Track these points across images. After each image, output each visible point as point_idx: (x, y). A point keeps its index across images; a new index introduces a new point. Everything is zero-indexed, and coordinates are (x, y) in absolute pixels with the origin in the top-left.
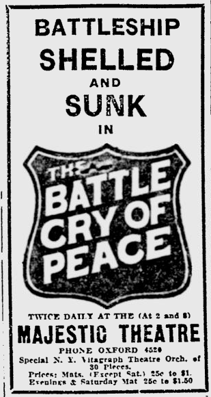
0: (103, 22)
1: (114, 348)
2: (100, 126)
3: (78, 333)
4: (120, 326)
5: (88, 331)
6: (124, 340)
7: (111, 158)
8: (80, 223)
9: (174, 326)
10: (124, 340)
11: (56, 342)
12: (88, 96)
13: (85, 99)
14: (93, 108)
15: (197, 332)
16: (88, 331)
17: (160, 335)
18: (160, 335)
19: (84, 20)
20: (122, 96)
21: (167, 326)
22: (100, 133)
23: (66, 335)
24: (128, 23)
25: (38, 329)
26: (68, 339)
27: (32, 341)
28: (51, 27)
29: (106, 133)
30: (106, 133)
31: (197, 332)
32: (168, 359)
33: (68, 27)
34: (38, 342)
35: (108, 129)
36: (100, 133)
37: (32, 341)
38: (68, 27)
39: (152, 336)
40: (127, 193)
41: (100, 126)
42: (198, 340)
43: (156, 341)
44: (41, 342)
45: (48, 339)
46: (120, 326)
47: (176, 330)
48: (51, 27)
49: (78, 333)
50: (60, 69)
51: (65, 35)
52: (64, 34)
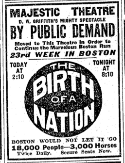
0: (72, 35)
1: (87, 139)
2: (114, 64)
3: (46, 12)
4: (72, 8)
8: (60, 77)
9: (101, 8)
11: (34, 16)
13: (66, 121)
17: (97, 31)
18: (97, 31)
20: (83, 8)
21: (98, 8)
23: (39, 13)
24: (40, 12)
27: (20, 15)
28: (20, 65)
34: (24, 17)
37: (20, 15)
39: (91, 12)
41: (114, 64)
42: (114, 14)
43: (92, 14)
44: (26, 16)
45: (30, 14)
46: (72, 8)
47: (102, 10)
48: (20, 65)
49: (46, 12)
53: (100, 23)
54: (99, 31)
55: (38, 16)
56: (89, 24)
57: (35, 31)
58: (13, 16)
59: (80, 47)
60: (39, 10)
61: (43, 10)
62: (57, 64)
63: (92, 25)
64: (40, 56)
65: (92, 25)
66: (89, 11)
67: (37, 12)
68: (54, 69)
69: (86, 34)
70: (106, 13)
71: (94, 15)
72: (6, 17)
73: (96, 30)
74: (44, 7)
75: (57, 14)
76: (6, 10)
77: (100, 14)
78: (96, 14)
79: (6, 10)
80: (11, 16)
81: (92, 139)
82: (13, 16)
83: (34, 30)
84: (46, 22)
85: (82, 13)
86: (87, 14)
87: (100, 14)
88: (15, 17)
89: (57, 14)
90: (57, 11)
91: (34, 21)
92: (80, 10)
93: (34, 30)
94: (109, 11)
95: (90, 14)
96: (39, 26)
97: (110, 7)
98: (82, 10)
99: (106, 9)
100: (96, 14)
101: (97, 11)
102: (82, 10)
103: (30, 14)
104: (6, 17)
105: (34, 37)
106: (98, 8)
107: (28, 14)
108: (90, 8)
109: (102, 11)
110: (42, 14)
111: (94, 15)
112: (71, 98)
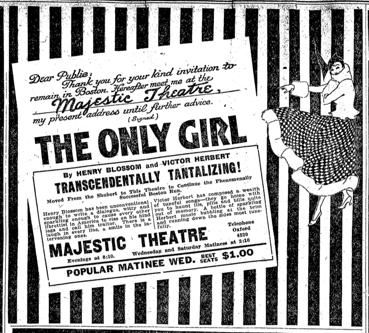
3: (103, 244)
5: (110, 243)
6: (144, 245)
7: (357, 112)
10: (144, 245)
12: (169, 124)
14: (90, 272)
16: (110, 243)
19: (235, 257)
22: (172, 179)
24: (94, 244)
25: (67, 245)
26: (94, 249)
29: (147, 267)
30: (147, 267)
32: (234, 230)
33: (134, 266)
35: (174, 261)
36: (172, 179)
38: (134, 266)
40: (163, 299)
43: (171, 243)
44: (71, 254)
45: (78, 250)
49: (103, 244)
50: (207, 239)
51: (251, 177)
52: (229, 154)
55: (90, 252)
58: (126, 184)
59: (171, 191)
60: (92, 242)
61: (99, 241)
66: (164, 238)
67: (88, 247)
69: (124, 183)
70: (193, 238)
71: (68, 255)
75: (121, 245)
77: (183, 241)
78: (177, 242)
80: (52, 256)
81: (110, 228)
82: (126, 184)
84: (80, 215)
85: (154, 243)
86: (162, 244)
87: (183, 241)
88: (123, 270)
89: (121, 245)
90: (121, 241)
92: (190, 234)
94: (198, 234)
95: (166, 243)
98: (153, 236)
99: (192, 233)
100: (177, 242)
101: (179, 236)
102: (153, 236)
103: (78, 250)
106: (134, 263)
107: (75, 251)
108: (165, 233)
109: (186, 235)
110: (97, 248)
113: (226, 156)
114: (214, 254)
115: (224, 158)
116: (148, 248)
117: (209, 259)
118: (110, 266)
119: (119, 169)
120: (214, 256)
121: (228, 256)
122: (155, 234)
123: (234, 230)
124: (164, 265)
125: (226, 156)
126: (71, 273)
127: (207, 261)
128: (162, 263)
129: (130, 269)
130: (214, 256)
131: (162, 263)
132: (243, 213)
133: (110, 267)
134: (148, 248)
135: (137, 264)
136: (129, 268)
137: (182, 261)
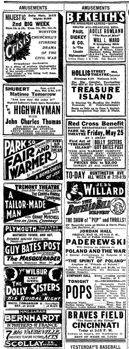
6: (44, 123)
10: (44, 123)
14: (14, 89)
15: (91, 315)
31: (91, 315)
38: (102, 75)
43: (95, 99)
53: (55, 105)
54: (54, 110)
56: (48, 105)
57: (70, 292)
62: (33, 228)
63: (50, 106)
64: (107, 244)
65: (50, 106)
68: (81, 208)
71: (96, 99)
72: (63, 106)
73: (53, 109)
74: (18, 14)
76: (66, 122)
79: (66, 122)
83: (69, 290)
91: (96, 138)
93: (69, 290)
96: (120, 125)
97: (20, 88)
104: (63, 106)
105: (82, 297)
111: (96, 99)
112: (44, 244)
113: (27, 89)
114: (66, 269)
115: (25, 90)
116: (45, 125)
117: (100, 74)
118: (111, 87)
119: (122, 261)
120: (92, 262)
121: (34, 218)
122: (37, 114)
123: (98, 261)
124: (119, 92)
125: (27, 89)
126: (69, 242)
127: (99, 75)
128: (118, 89)
129: (120, 253)
130: (92, 262)
131: (118, 89)
132: (115, 255)
133: (111, 88)
134: (45, 125)
135: (103, 250)
136: (119, 252)
137: (88, 242)
